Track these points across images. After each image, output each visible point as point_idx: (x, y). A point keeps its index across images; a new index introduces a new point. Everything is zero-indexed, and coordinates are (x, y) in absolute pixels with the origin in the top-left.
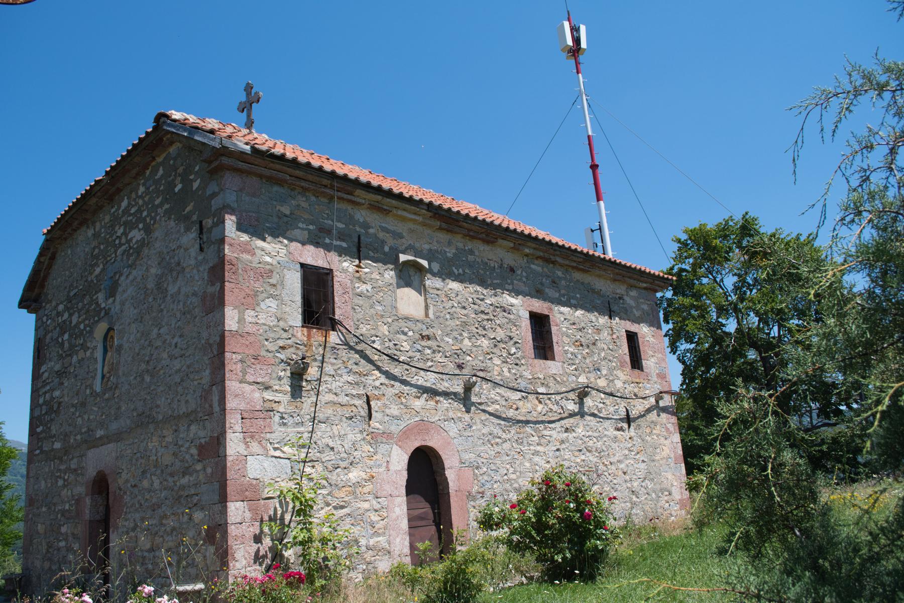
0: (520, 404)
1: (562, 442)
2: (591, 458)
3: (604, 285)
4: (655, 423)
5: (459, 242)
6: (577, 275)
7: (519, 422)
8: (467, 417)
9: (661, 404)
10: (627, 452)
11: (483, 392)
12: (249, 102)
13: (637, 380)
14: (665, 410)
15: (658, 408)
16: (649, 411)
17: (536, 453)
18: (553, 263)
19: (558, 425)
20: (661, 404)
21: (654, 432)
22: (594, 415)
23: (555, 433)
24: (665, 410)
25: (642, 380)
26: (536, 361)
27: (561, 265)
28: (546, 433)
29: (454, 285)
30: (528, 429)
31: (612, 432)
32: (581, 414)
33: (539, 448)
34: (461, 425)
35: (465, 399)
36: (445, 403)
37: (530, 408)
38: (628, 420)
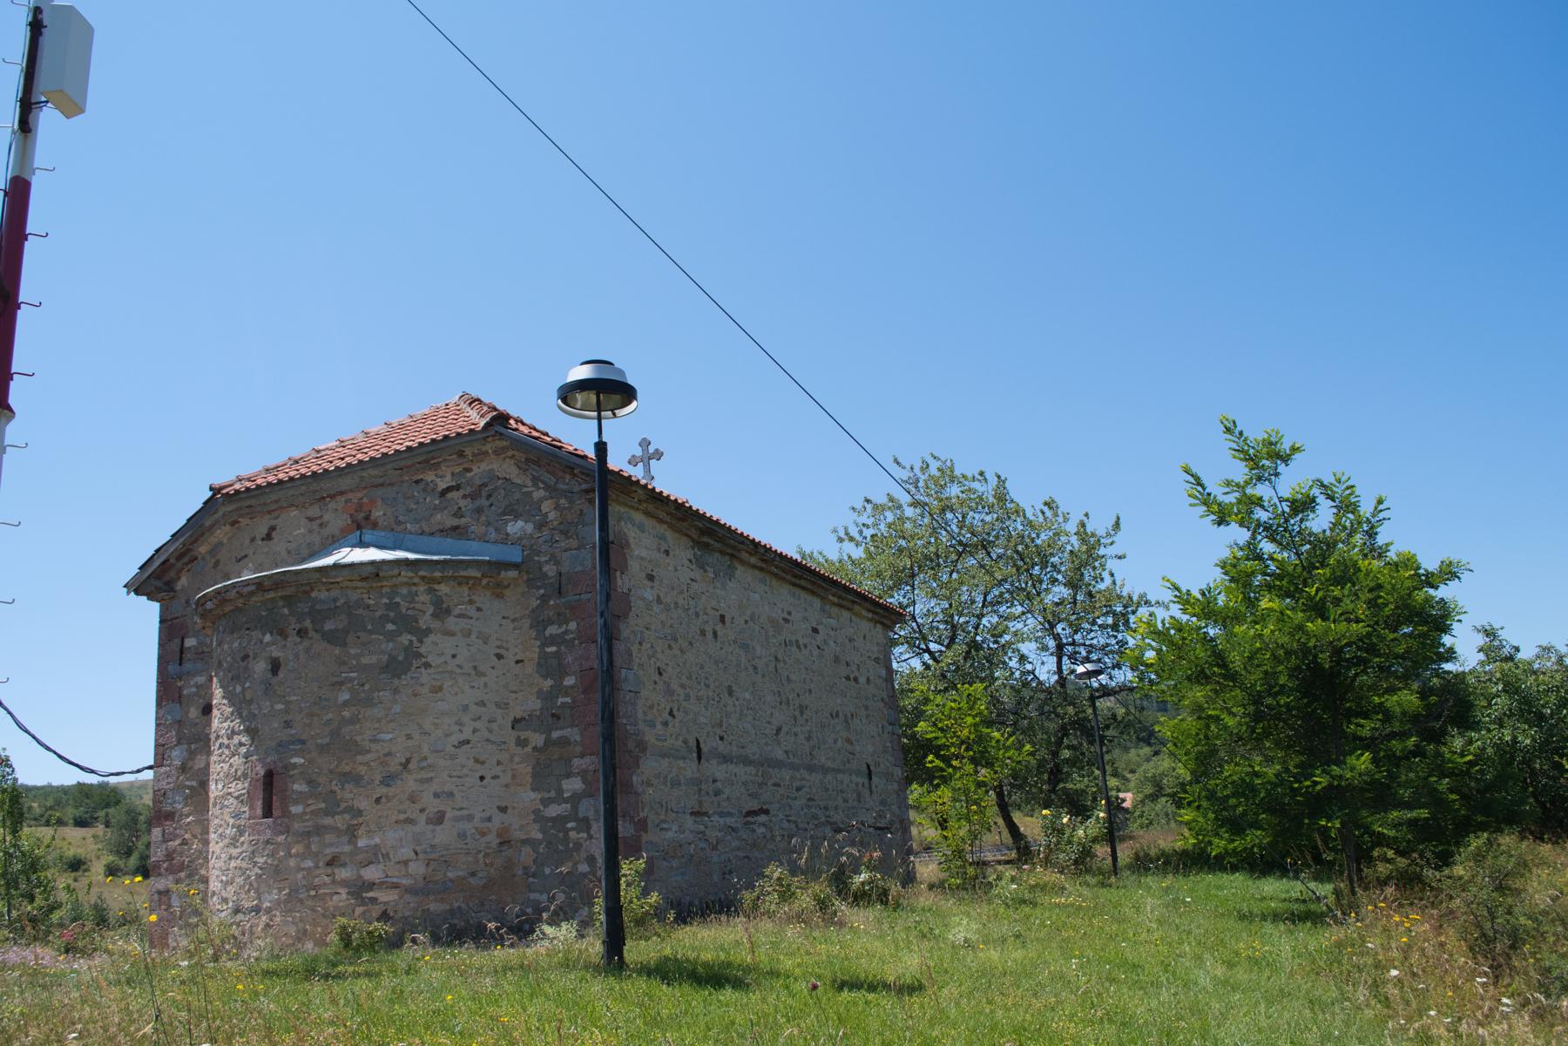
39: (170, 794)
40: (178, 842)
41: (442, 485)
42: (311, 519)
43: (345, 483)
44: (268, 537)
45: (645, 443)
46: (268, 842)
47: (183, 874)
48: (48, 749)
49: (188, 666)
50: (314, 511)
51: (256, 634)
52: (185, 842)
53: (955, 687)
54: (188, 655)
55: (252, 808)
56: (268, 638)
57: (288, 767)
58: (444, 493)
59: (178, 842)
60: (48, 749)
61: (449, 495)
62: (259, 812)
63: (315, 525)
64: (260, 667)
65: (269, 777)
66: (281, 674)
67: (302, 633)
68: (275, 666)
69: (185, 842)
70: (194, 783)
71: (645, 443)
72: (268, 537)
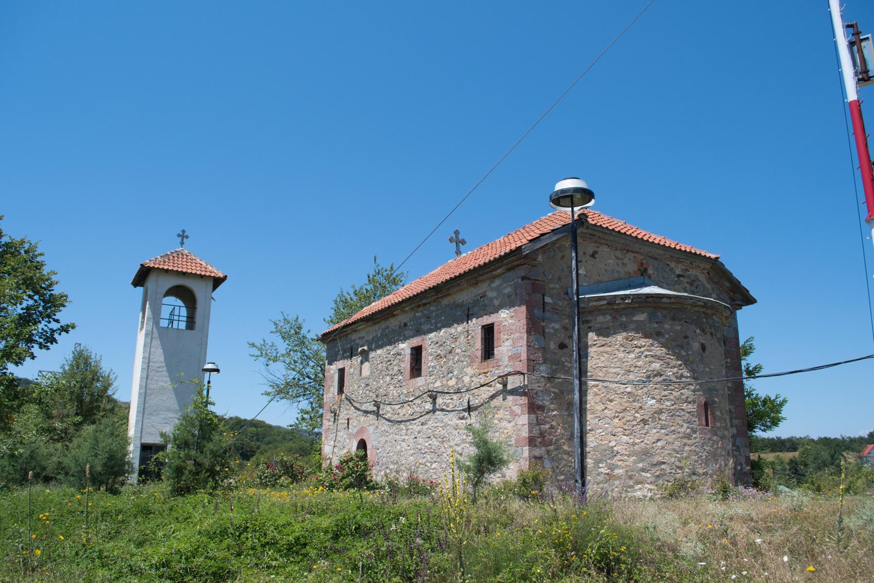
0: (400, 411)
1: (419, 432)
2: (435, 443)
3: (465, 296)
4: (498, 408)
5: (383, 325)
6: (445, 301)
7: (398, 422)
8: (376, 423)
9: (509, 387)
10: (464, 437)
11: (386, 410)
12: (458, 242)
13: (485, 371)
14: (514, 392)
15: (506, 392)
16: (493, 397)
17: (404, 440)
18: (425, 304)
19: (417, 421)
20: (509, 387)
21: (496, 416)
22: (442, 410)
23: (415, 427)
24: (514, 392)
25: (491, 369)
26: (496, 357)
27: (429, 303)
28: (410, 427)
29: (379, 352)
30: (402, 426)
31: (456, 421)
32: (434, 411)
33: (406, 437)
34: (374, 427)
35: (377, 414)
36: (371, 416)
37: (406, 412)
38: (469, 409)
39: (540, 394)
40: (547, 426)
41: (678, 272)
42: (618, 258)
43: (637, 247)
44: (593, 256)
45: (184, 231)
46: (709, 439)
47: (552, 447)
48: (869, 357)
49: (548, 315)
50: (618, 254)
51: (692, 327)
52: (552, 427)
53: (652, 540)
54: (547, 308)
55: (699, 420)
56: (698, 331)
57: (714, 402)
58: (679, 276)
59: (547, 426)
60: (869, 357)
61: (681, 279)
62: (704, 423)
63: (620, 262)
64: (696, 346)
65: (706, 405)
66: (707, 352)
67: (711, 334)
68: (703, 347)
69: (552, 427)
70: (557, 391)
71: (184, 231)
72: (593, 256)
